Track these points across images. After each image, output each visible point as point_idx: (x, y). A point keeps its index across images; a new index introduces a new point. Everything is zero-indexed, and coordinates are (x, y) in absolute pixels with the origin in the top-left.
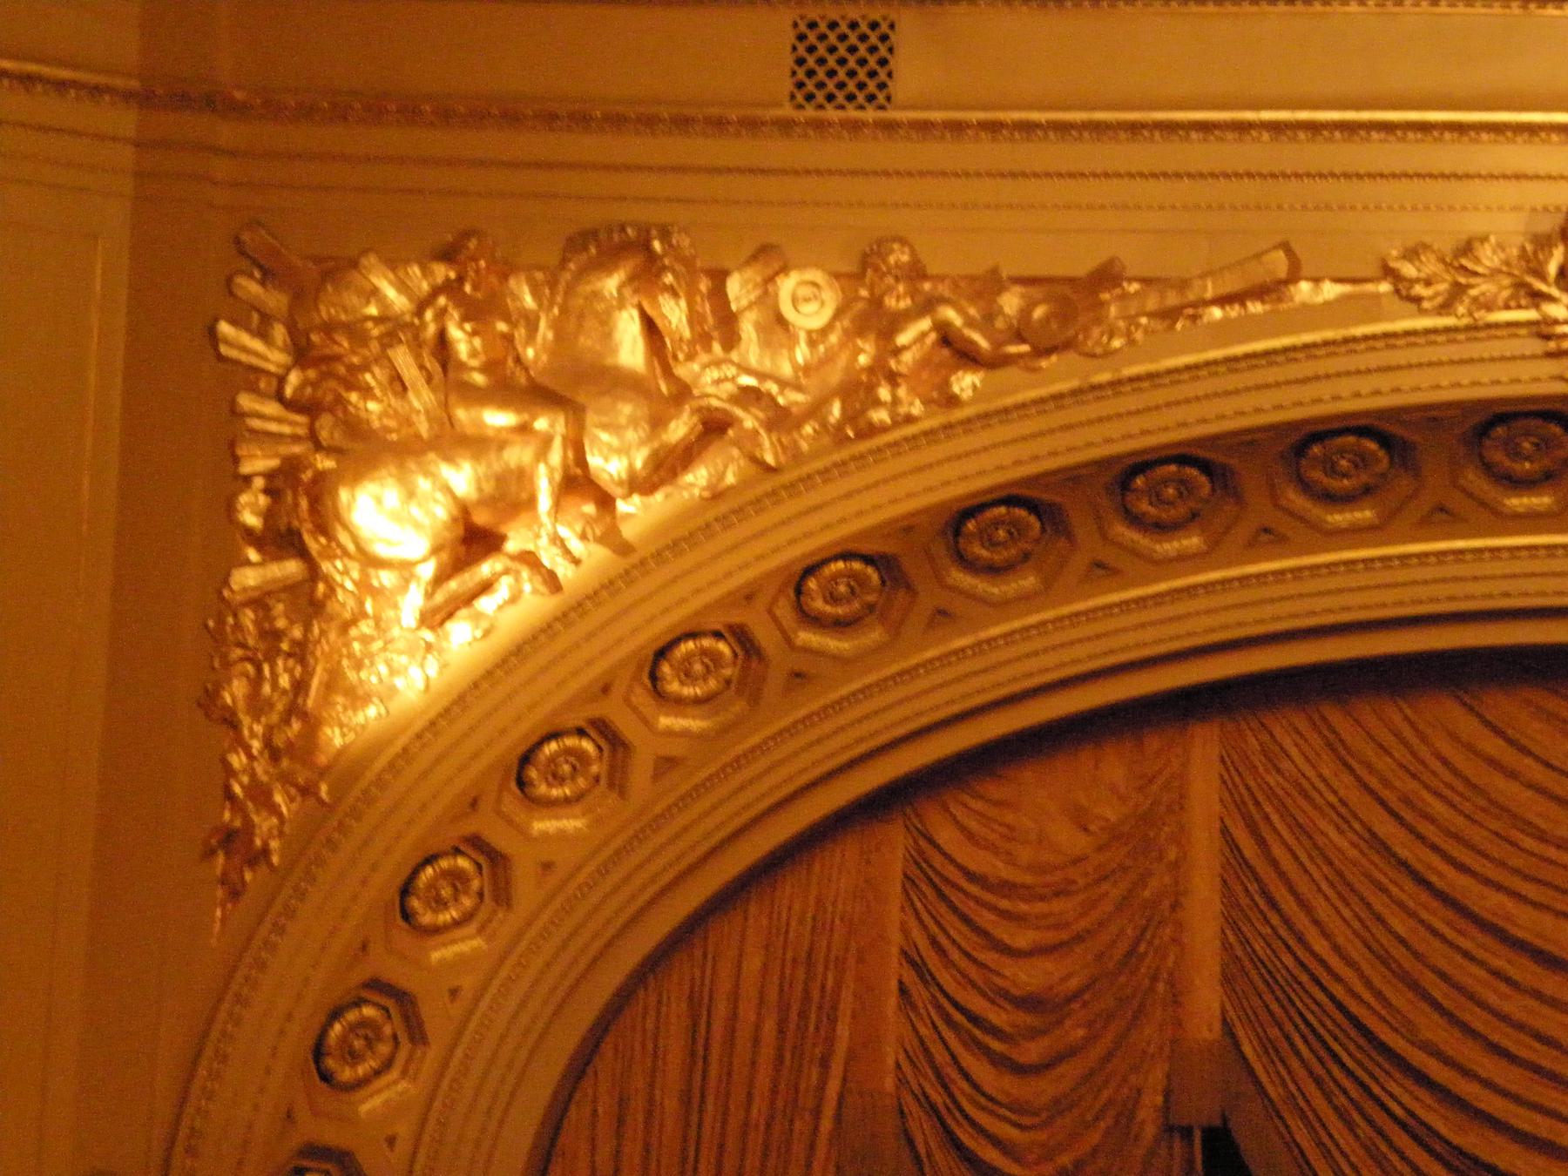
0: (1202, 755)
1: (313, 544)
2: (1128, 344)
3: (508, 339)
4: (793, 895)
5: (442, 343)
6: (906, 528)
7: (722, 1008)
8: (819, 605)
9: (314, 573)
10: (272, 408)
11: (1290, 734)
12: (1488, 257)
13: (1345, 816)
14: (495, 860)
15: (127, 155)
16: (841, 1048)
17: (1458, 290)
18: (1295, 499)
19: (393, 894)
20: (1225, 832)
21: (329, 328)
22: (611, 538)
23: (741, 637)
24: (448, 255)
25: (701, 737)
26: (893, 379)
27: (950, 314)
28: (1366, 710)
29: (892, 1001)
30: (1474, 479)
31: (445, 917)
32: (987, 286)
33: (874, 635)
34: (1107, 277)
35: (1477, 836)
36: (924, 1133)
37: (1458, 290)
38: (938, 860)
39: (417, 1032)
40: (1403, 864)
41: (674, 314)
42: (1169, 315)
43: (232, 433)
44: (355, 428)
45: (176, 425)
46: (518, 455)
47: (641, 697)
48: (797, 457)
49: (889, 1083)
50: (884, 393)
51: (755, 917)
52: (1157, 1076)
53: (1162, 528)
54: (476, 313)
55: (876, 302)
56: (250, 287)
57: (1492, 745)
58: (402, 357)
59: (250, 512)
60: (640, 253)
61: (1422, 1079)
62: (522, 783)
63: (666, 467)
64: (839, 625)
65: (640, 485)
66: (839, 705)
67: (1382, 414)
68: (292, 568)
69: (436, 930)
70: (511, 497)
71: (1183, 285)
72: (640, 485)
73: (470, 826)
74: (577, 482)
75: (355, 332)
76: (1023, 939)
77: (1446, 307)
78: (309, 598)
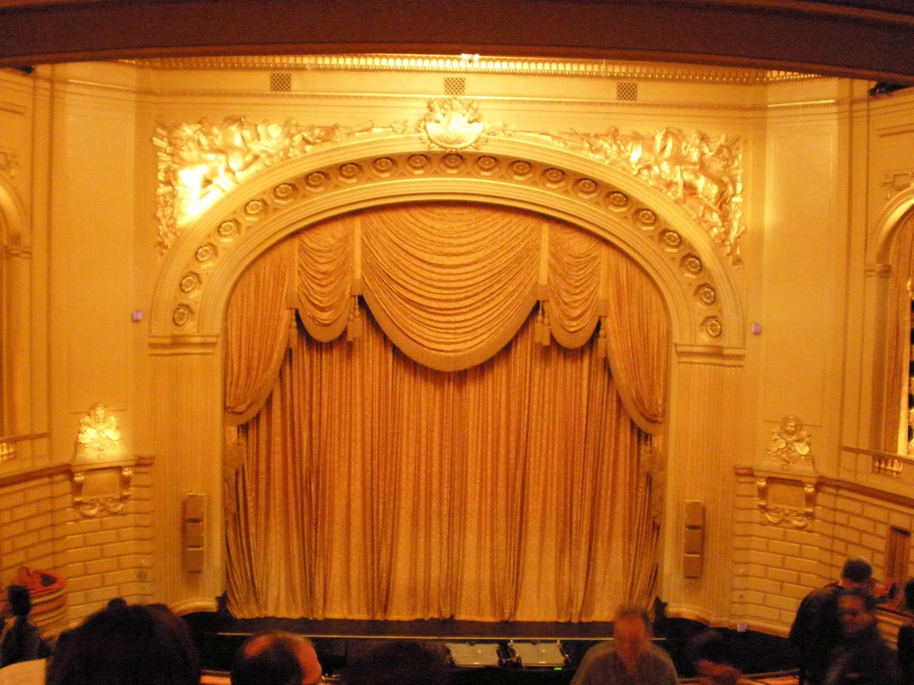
0: (358, 222)
1: (174, 183)
2: (341, 140)
3: (212, 140)
4: (276, 253)
5: (199, 143)
6: (296, 178)
7: (262, 276)
8: (279, 194)
9: (174, 189)
10: (164, 155)
11: (374, 218)
12: (410, 124)
13: (385, 235)
14: (214, 247)
15: (836, 116)
17: (404, 130)
18: (375, 172)
19: (178, 286)
21: (175, 138)
22: (235, 180)
23: (263, 201)
24: (200, 123)
25: (255, 222)
26: (293, 147)
27: (305, 134)
29: (296, 273)
30: (408, 168)
31: (190, 289)
32: (312, 128)
33: (290, 201)
34: (336, 126)
35: (410, 238)
36: (304, 300)
37: (404, 130)
39: (200, 282)
40: (395, 244)
41: (247, 134)
42: (349, 134)
43: (157, 161)
44: (182, 159)
45: (146, 160)
46: (215, 164)
47: (243, 214)
48: (273, 163)
49: (296, 290)
50: (291, 150)
51: (268, 259)
52: (349, 286)
53: (349, 178)
54: (206, 134)
55: (289, 131)
56: (159, 130)
57: (412, 220)
58: (191, 144)
59: (161, 176)
60: (239, 121)
61: (399, 284)
62: (219, 232)
63: (247, 166)
64: (283, 198)
66: (284, 215)
67: (393, 155)
68: (169, 188)
69: (189, 292)
70: (215, 173)
71: (351, 128)
72: (242, 170)
73: (209, 241)
74: (228, 170)
75: (181, 139)
76: (323, 261)
77: (402, 133)
78: (173, 195)
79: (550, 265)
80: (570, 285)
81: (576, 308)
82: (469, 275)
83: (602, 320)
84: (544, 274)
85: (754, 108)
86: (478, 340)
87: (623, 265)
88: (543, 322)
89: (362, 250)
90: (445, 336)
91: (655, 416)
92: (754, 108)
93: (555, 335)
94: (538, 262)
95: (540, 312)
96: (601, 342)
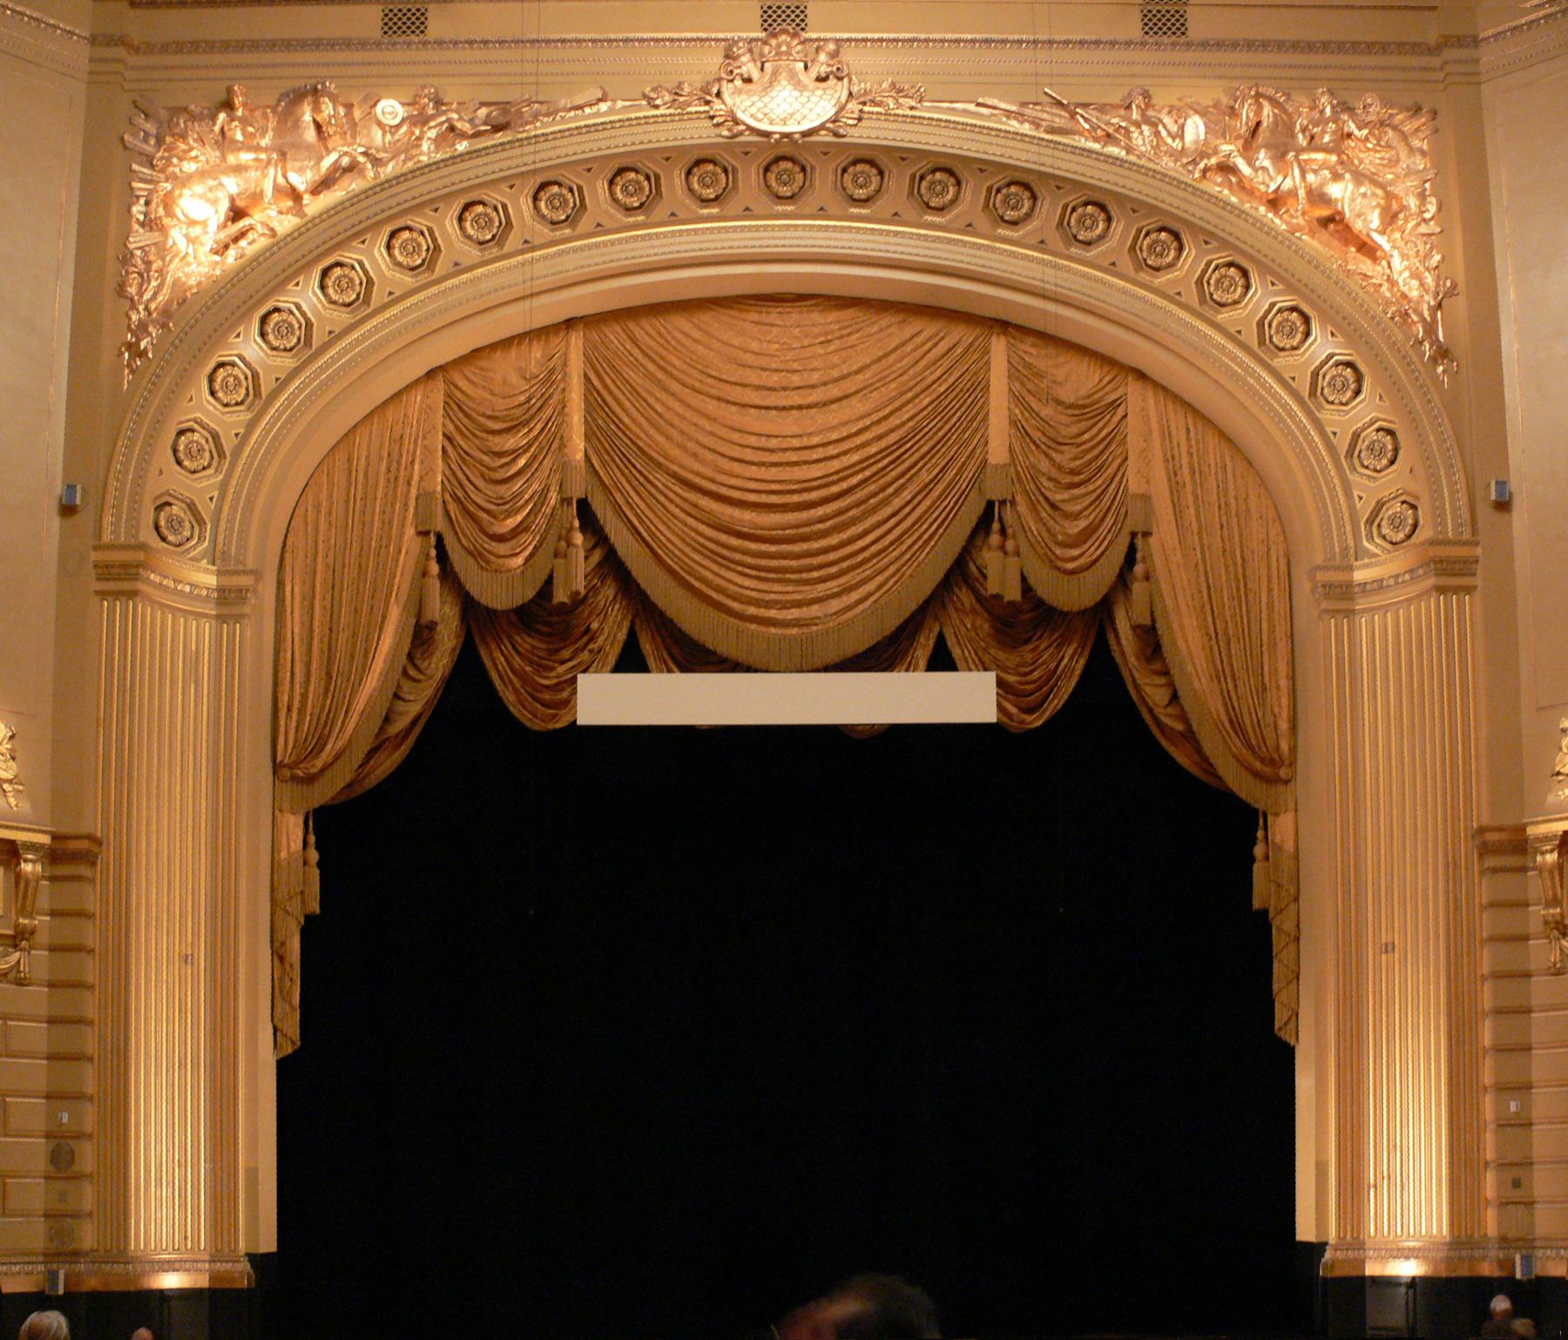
0: (576, 342)
11: (614, 334)
16: (416, 477)
20: (585, 375)
28: (645, 323)
38: (457, 394)
49: (439, 488)
57: (697, 334)
65: (316, 190)
68: (155, 236)
70: (257, 197)
79: (1013, 422)
80: (1060, 468)
81: (1077, 516)
82: (832, 450)
83: (1139, 541)
84: (998, 443)
85: (1448, 41)
86: (855, 596)
87: (1178, 421)
88: (1002, 547)
89: (586, 400)
90: (777, 587)
91: (1272, 763)
92: (1448, 41)
93: (1032, 581)
94: (985, 419)
95: (996, 526)
96: (1138, 588)
